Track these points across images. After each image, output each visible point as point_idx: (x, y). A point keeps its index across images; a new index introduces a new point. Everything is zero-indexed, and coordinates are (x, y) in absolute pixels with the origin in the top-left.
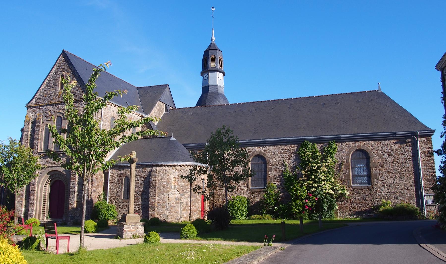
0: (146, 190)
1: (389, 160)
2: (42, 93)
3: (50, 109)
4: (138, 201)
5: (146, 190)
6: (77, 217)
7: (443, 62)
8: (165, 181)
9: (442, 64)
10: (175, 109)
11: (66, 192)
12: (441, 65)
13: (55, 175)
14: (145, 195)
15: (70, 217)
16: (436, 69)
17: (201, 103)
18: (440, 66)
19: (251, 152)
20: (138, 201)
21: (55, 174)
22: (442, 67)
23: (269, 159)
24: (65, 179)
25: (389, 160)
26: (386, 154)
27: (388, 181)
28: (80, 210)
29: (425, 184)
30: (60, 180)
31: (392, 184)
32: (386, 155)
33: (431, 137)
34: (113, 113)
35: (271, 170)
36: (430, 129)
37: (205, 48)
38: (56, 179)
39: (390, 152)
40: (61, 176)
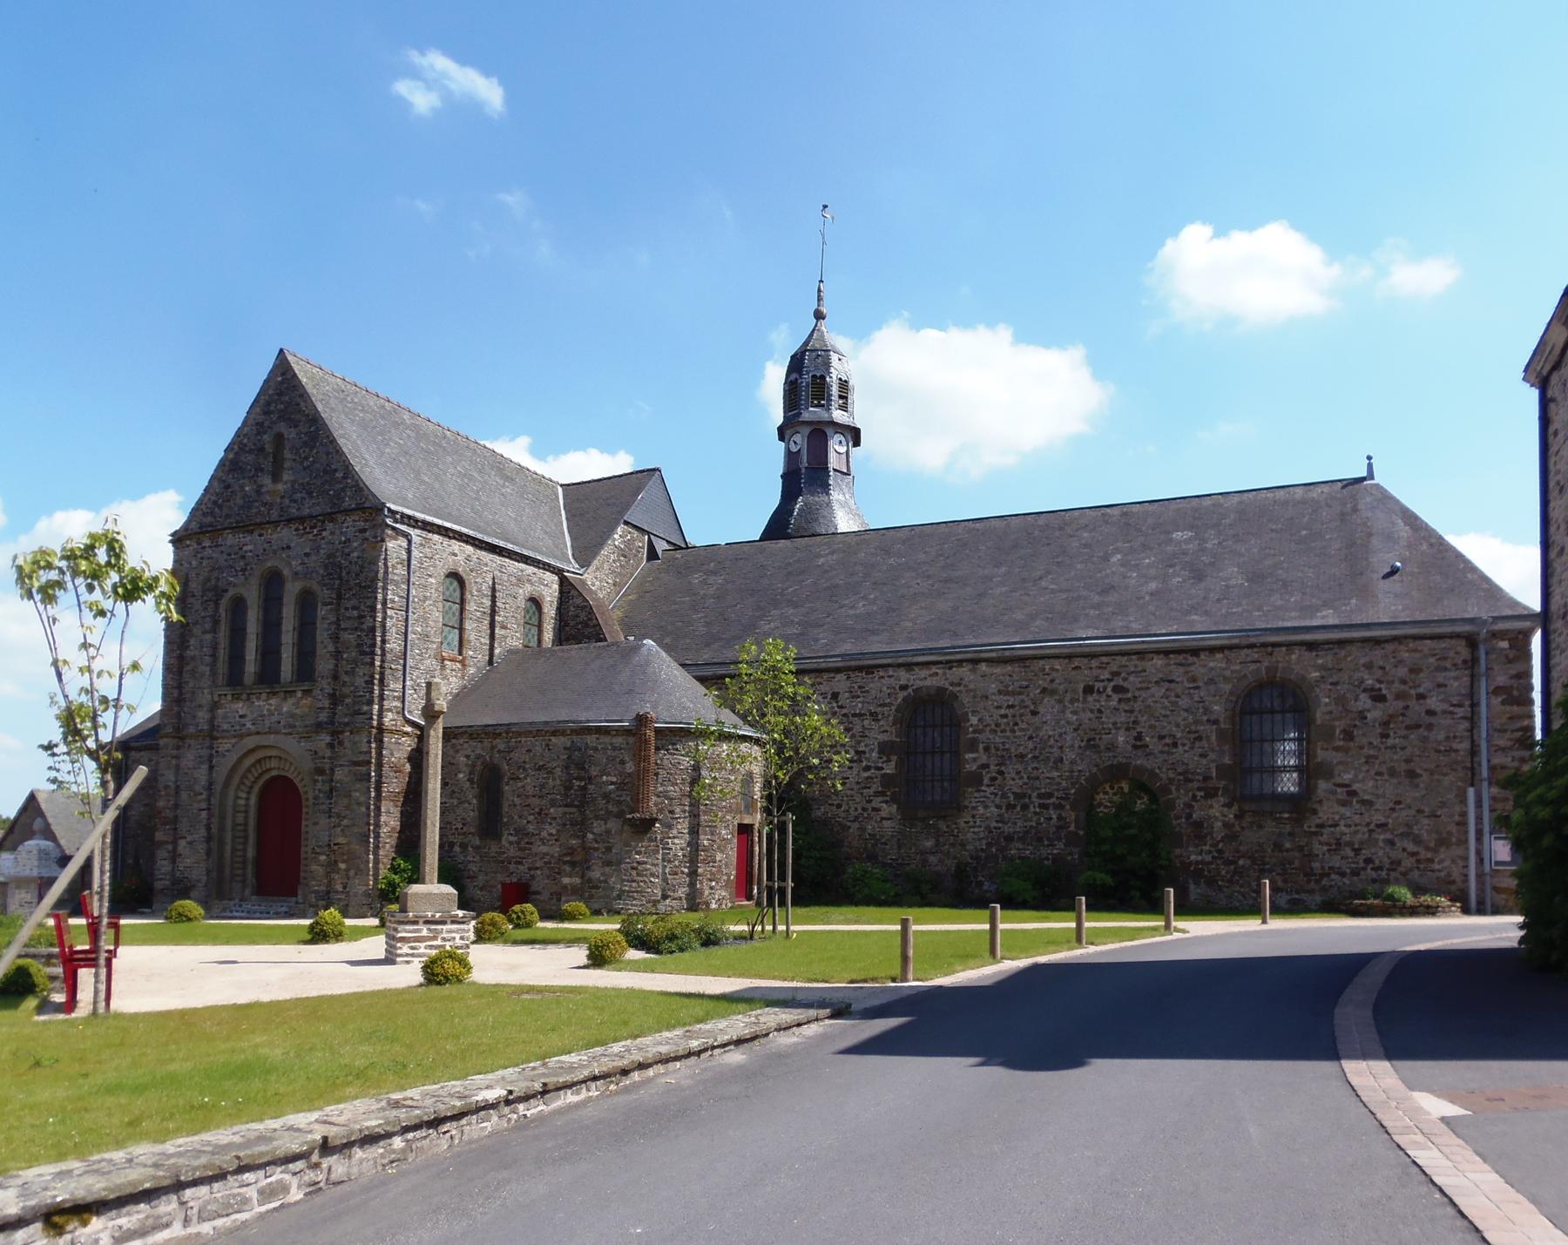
0: (552, 810)
1: (1376, 714)
2: (217, 494)
3: (245, 548)
4: (527, 843)
5: (552, 810)
6: (337, 892)
7: (1544, 351)
8: (614, 779)
9: (1543, 360)
10: (681, 547)
11: (304, 816)
12: (1541, 365)
13: (267, 760)
14: (551, 824)
15: (315, 892)
16: (1523, 379)
17: (778, 527)
18: (1539, 368)
19: (910, 690)
20: (527, 843)
21: (270, 757)
22: (1545, 372)
23: (967, 713)
24: (299, 774)
25: (1376, 714)
26: (1363, 697)
27: (1365, 788)
28: (345, 870)
29: (1494, 799)
30: (285, 778)
31: (1378, 796)
32: (1364, 701)
33: (110, 699)
34: (454, 560)
35: (973, 745)
36: (1509, 612)
37: (795, 347)
38: (274, 773)
39: (1380, 689)
40: (288, 764)
